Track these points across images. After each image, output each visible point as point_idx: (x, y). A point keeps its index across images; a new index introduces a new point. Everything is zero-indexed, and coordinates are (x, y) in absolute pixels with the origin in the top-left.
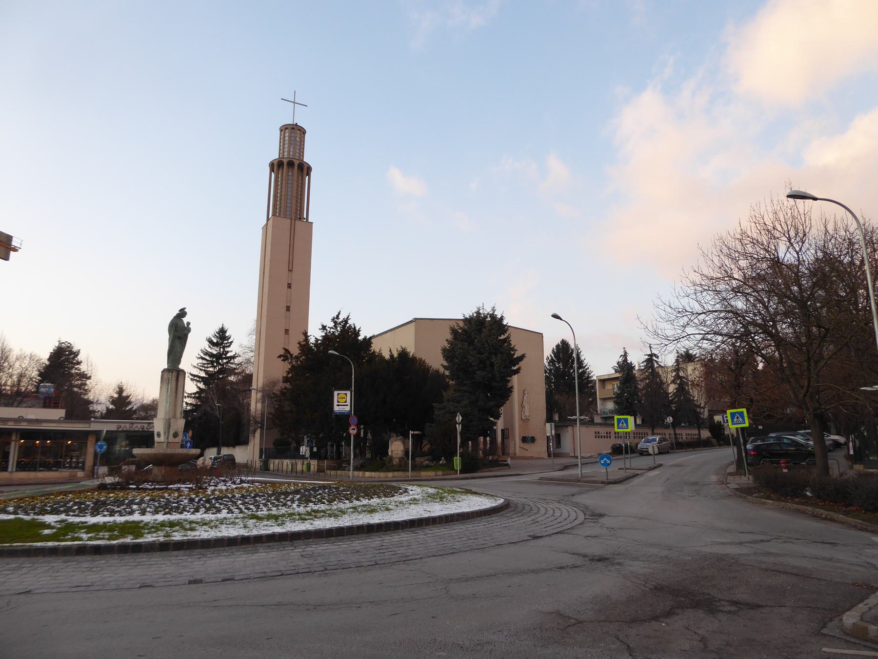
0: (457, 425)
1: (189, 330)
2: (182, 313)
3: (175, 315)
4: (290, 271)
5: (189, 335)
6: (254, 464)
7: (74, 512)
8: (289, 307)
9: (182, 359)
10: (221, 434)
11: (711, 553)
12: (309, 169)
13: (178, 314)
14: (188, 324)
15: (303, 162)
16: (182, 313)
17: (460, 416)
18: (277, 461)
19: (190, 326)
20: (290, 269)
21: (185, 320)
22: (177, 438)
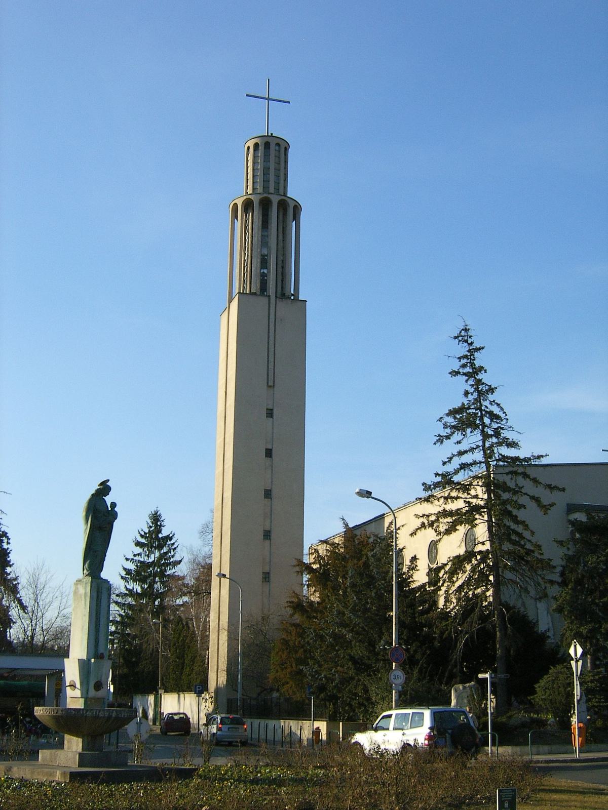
0: (573, 663)
1: (114, 516)
2: (104, 489)
3: (93, 492)
4: (270, 386)
5: (114, 523)
6: (238, 224)
7: (363, 627)
8: (271, 450)
9: (105, 563)
10: (429, 670)
11: (569, 770)
12: (297, 208)
13: (98, 491)
14: (114, 505)
15: (286, 199)
16: (104, 489)
17: (578, 647)
18: (256, 722)
19: (116, 509)
20: (271, 383)
21: (109, 499)
22: (100, 691)
